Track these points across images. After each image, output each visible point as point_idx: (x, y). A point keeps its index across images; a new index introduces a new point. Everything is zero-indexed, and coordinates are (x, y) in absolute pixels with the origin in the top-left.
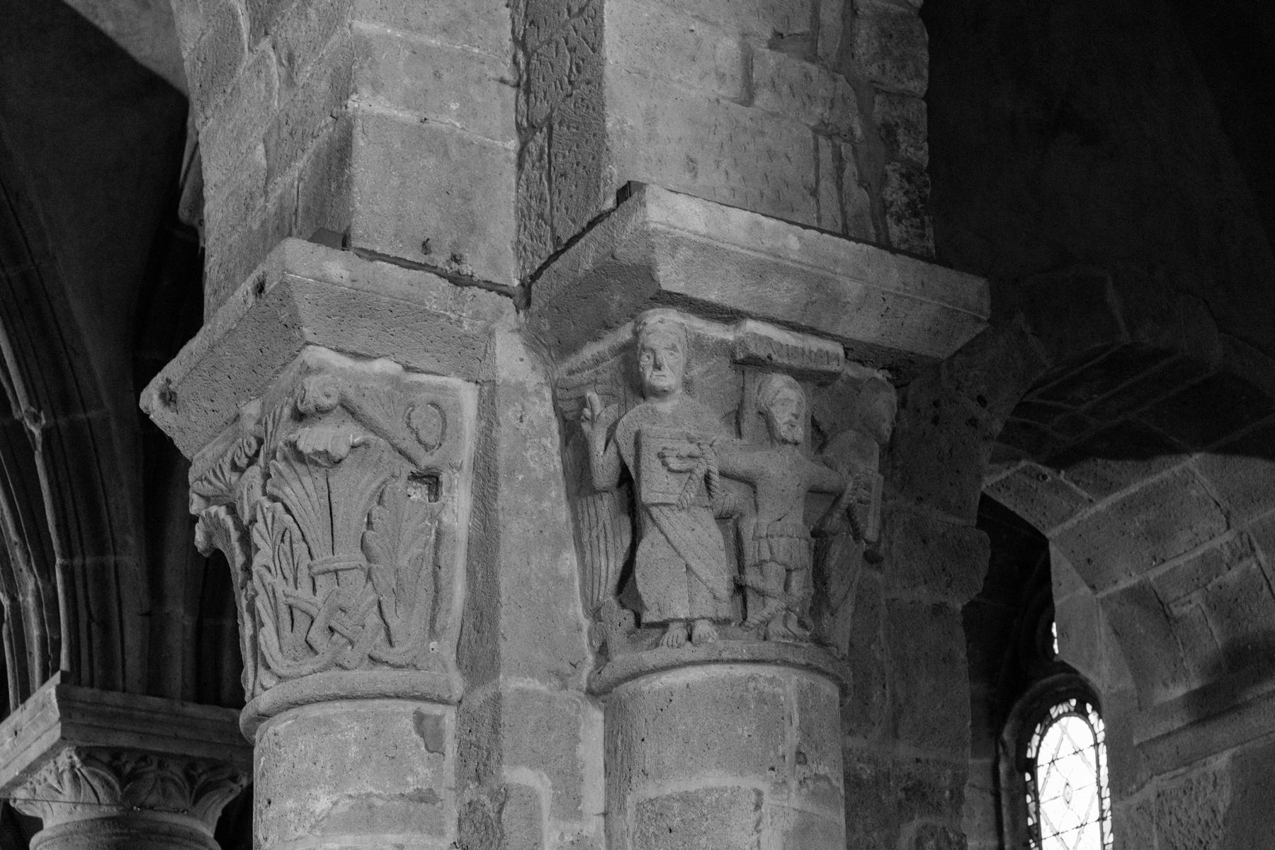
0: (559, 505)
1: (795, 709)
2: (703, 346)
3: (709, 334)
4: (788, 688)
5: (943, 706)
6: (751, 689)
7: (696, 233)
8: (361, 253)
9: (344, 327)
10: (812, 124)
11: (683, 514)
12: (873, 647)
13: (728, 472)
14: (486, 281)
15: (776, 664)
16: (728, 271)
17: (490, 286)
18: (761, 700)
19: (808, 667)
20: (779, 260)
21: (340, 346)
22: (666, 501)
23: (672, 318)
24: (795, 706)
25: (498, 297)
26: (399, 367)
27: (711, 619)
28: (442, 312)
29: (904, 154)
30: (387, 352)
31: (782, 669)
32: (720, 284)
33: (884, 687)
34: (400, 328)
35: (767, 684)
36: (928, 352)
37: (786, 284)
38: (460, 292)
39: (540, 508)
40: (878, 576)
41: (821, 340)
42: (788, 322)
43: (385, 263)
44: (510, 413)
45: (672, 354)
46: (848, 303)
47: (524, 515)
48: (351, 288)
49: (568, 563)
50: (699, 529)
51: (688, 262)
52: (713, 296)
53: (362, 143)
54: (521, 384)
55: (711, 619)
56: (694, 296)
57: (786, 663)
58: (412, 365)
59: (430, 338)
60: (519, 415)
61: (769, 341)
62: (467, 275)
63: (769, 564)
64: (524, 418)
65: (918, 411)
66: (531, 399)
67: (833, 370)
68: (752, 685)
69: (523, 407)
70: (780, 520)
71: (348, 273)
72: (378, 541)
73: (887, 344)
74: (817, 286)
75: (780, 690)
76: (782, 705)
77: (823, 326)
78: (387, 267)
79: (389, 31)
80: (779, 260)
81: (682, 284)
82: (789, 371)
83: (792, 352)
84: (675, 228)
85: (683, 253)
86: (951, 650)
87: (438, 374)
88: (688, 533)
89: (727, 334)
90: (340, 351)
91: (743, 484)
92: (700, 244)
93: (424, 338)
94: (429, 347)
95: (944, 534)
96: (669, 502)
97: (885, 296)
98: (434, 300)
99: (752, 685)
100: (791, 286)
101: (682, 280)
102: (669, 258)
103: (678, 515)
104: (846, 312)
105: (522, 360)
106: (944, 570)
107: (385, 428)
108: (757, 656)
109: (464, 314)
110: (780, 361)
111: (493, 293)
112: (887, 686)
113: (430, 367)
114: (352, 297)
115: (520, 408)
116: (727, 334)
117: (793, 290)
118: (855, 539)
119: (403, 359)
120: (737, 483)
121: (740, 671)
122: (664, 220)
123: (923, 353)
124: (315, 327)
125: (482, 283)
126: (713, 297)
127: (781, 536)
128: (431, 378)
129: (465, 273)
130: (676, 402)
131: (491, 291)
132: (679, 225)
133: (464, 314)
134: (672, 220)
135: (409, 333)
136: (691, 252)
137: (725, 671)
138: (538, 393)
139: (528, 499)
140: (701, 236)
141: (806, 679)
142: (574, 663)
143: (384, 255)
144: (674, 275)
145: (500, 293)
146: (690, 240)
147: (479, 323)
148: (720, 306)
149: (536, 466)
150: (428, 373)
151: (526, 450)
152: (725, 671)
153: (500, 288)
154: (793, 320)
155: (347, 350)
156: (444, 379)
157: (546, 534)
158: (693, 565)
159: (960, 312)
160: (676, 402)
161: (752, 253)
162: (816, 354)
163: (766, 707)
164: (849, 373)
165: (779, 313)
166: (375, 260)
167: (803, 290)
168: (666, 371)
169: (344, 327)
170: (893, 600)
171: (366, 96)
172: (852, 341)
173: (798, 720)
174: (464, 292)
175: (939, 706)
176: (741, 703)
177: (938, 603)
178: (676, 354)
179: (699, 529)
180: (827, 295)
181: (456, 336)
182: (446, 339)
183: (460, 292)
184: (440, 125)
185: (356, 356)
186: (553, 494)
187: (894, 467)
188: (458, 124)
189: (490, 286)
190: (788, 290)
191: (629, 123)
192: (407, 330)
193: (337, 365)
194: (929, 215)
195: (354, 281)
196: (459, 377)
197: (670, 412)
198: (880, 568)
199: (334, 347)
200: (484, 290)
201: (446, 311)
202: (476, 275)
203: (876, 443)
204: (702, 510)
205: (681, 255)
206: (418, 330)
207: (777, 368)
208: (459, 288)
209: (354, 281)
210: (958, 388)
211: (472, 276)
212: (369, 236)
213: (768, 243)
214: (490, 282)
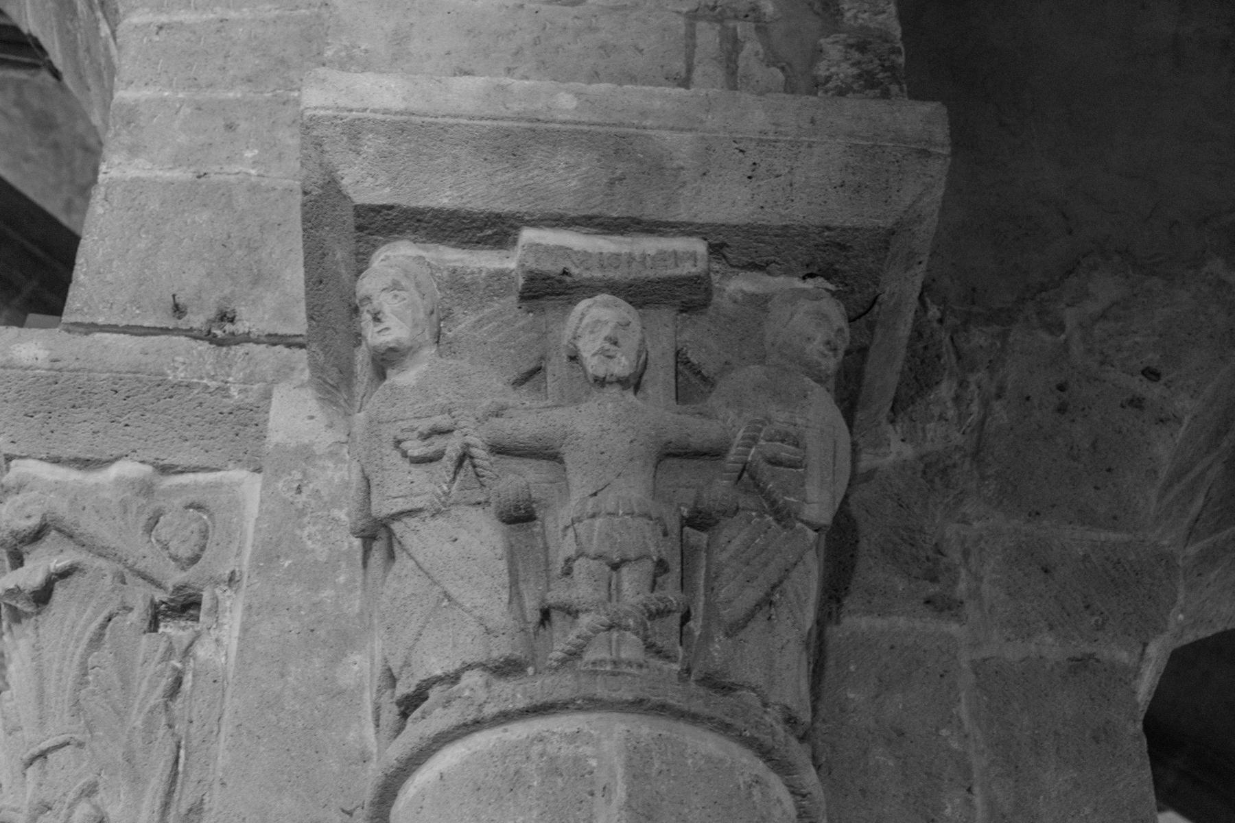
0: (350, 591)
1: (619, 777)
2: (466, 286)
3: (472, 265)
4: (607, 745)
5: (1095, 810)
6: (534, 756)
7: (386, 112)
8: (71, 328)
9: (53, 426)
10: (685, 10)
11: (440, 521)
12: (944, 732)
13: (506, 442)
14: (269, 335)
15: (580, 709)
16: (456, 157)
17: (274, 340)
18: (553, 769)
19: (638, 706)
20: (534, 125)
21: (54, 453)
22: (408, 507)
23: (402, 252)
24: (620, 771)
25: (286, 351)
26: (148, 469)
27: (483, 666)
28: (195, 380)
29: (852, 23)
30: (124, 451)
31: (594, 716)
32: (450, 180)
33: (969, 790)
34: (137, 414)
35: (564, 745)
36: (857, 222)
37: (562, 159)
38: (227, 353)
39: (315, 599)
40: (954, 628)
41: (662, 239)
42: (590, 218)
43: (107, 335)
44: (280, 485)
45: (396, 296)
46: (682, 168)
47: (285, 612)
48: (50, 370)
49: (356, 668)
50: (464, 537)
51: (384, 156)
52: (445, 200)
53: (100, 211)
54: (306, 447)
55: (483, 666)
56: (413, 204)
57: (593, 704)
58: (166, 462)
59: (186, 420)
60: (296, 485)
61: (565, 251)
62: (244, 333)
63: (577, 562)
64: (304, 489)
65: (1028, 398)
66: (320, 463)
67: (685, 273)
68: (537, 748)
69: (304, 474)
70: (595, 494)
71: (47, 352)
72: (97, 698)
73: (776, 221)
74: (616, 152)
75: (589, 750)
76: (591, 773)
77: (651, 210)
78: (109, 338)
79: (166, 94)
80: (534, 125)
81: (388, 190)
82: (612, 288)
83: (604, 261)
84: (351, 110)
85: (371, 144)
86: (1108, 722)
87: (212, 470)
88: (448, 546)
89: (507, 262)
90: (57, 461)
91: (544, 463)
92: (394, 123)
93: (177, 422)
94: (186, 434)
95: (1086, 557)
96: (414, 507)
97: (742, 146)
98: (182, 368)
99: (537, 748)
100: (572, 161)
101: (384, 186)
102: (352, 156)
103: (432, 524)
104: (685, 183)
105: (312, 418)
106: (1087, 607)
107: (113, 546)
108: (539, 699)
109: (231, 379)
110: (586, 275)
111: (278, 348)
112: (976, 790)
113: (194, 461)
114: (50, 380)
115: (298, 476)
116: (507, 262)
117: (577, 166)
118: (778, 521)
119: (151, 455)
120: (534, 462)
121: (519, 731)
122: (330, 103)
123: (848, 224)
124: (11, 433)
125: (263, 339)
126: (446, 201)
127: (593, 516)
128: (201, 477)
129: (241, 332)
130: (424, 367)
131: (275, 345)
132: (355, 105)
133: (231, 379)
134: (343, 102)
135: (152, 418)
136: (383, 140)
137: (495, 737)
138: (332, 455)
139: (295, 590)
140: (396, 113)
141: (646, 728)
142: (348, 809)
143: (109, 326)
144: (370, 179)
145: (289, 346)
146: (374, 121)
147: (256, 387)
148: (463, 213)
149: (317, 547)
150: (195, 470)
151: (302, 527)
152: (495, 737)
153: (291, 340)
154: (595, 211)
155: (65, 456)
156: (219, 474)
157: (321, 633)
158: (452, 590)
159: (887, 146)
160: (424, 367)
161: (489, 123)
162: (653, 258)
163: (559, 780)
164: (745, 289)
165: (566, 205)
166: (91, 332)
167: (595, 163)
168: (390, 320)
169: (53, 426)
170: (985, 660)
171: (117, 162)
172: (716, 228)
173: (623, 795)
174: (232, 353)
175: (1087, 810)
176: (516, 781)
177: (1080, 657)
178: (403, 294)
179: (464, 537)
180: (640, 162)
181: (225, 410)
182: (208, 418)
183: (227, 353)
184: (227, 177)
185: (85, 464)
186: (342, 579)
187: (983, 478)
188: (253, 172)
189: (274, 340)
190: (569, 167)
191: (363, 48)
192: (148, 415)
193: (50, 478)
194: (899, 83)
195: (56, 361)
196: (242, 467)
197: (414, 383)
198: (960, 620)
199: (44, 456)
200: (265, 345)
201: (202, 378)
202: (254, 330)
203: (807, 379)
204: (472, 509)
205: (369, 147)
206: (164, 412)
207: (589, 289)
208: (225, 349)
209: (56, 361)
210: (1102, 363)
211: (249, 333)
212: (90, 308)
213: (516, 107)
214: (276, 335)
